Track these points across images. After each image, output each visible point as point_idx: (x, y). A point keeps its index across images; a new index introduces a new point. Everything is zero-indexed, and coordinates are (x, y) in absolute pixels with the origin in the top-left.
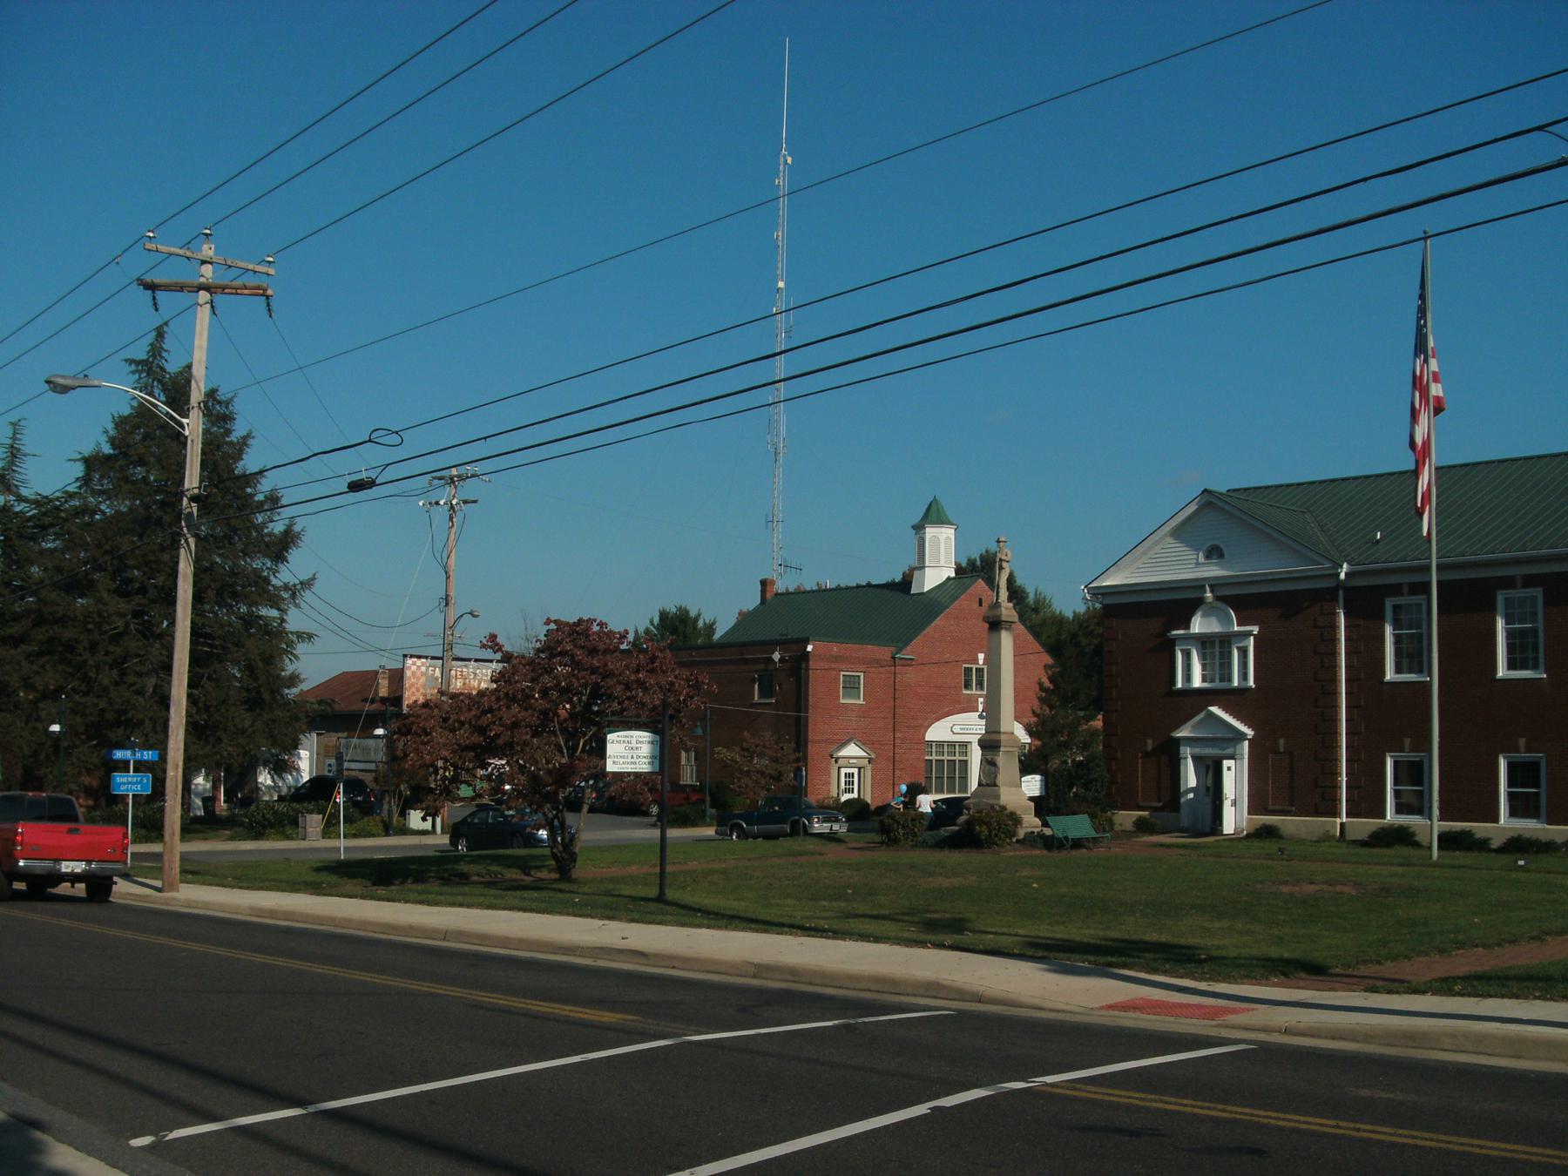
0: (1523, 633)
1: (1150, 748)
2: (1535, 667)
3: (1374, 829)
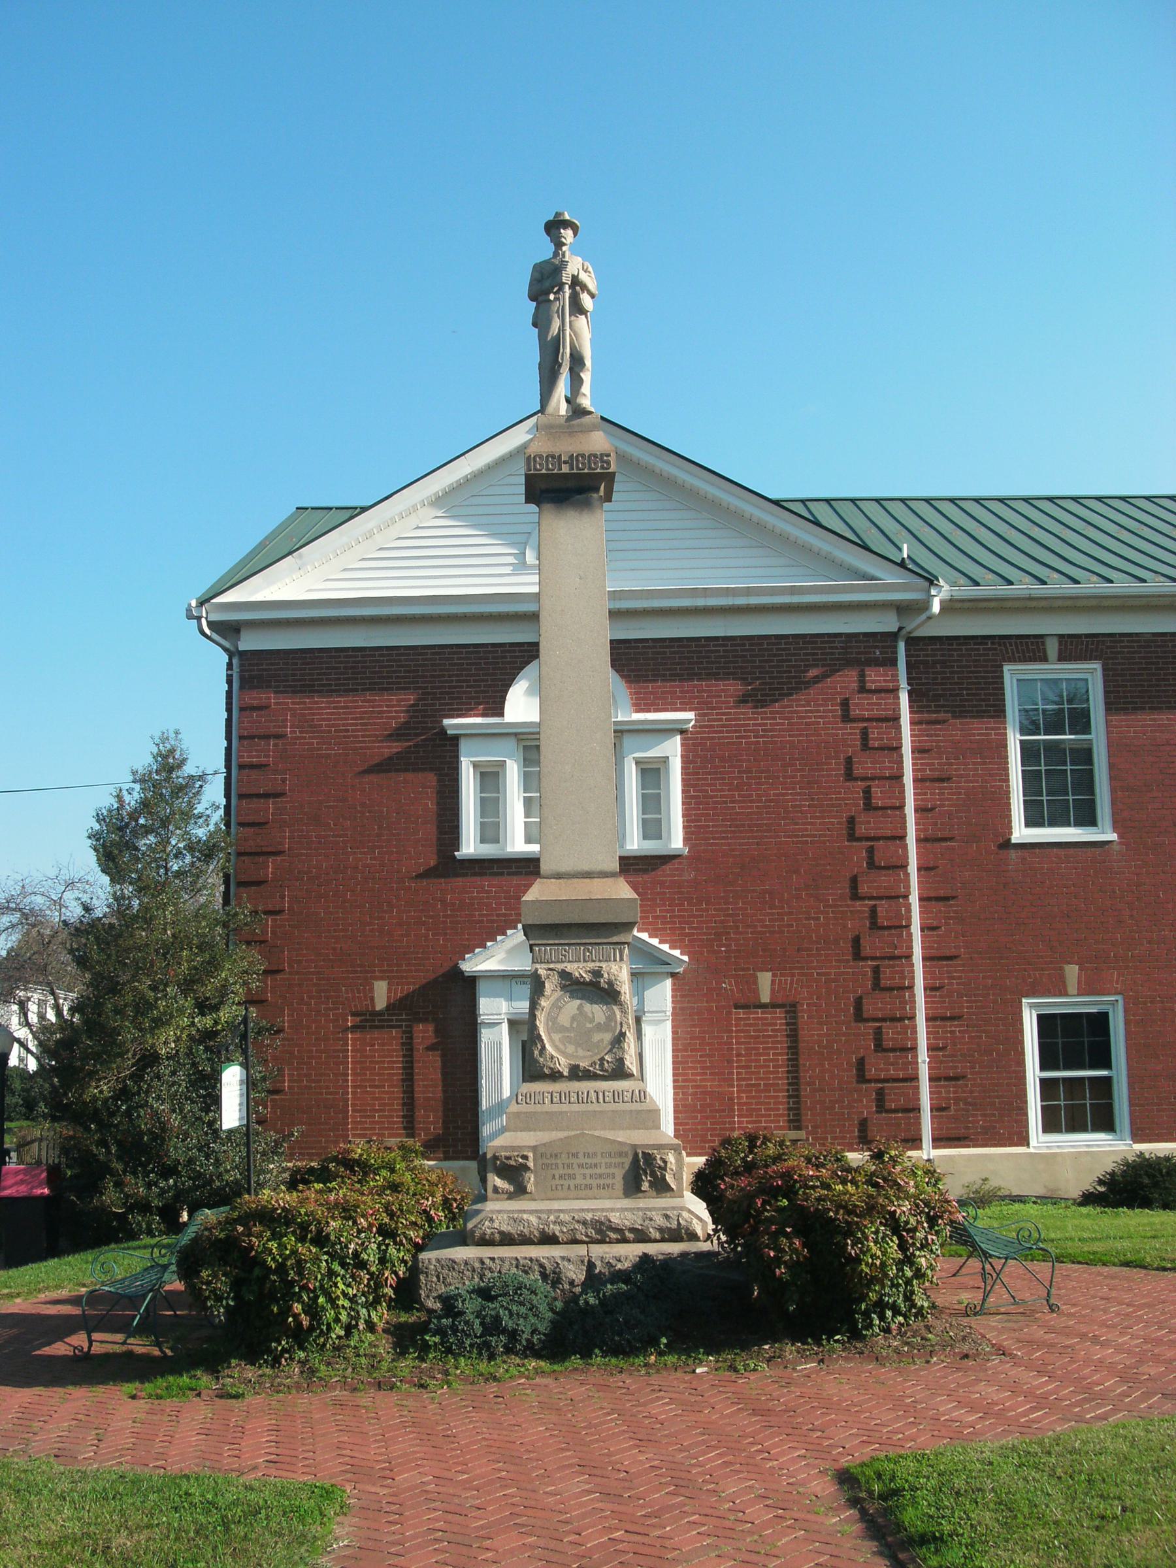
0: (1055, 752)
1: (381, 1004)
2: (1088, 818)
3: (1108, 1166)
